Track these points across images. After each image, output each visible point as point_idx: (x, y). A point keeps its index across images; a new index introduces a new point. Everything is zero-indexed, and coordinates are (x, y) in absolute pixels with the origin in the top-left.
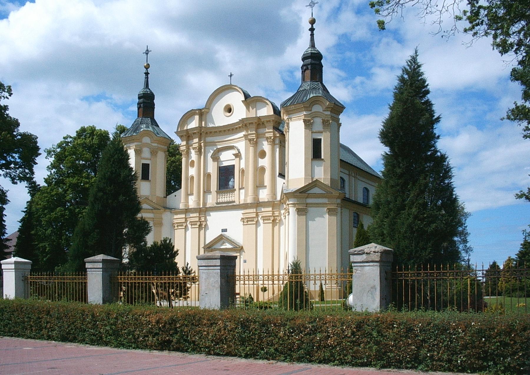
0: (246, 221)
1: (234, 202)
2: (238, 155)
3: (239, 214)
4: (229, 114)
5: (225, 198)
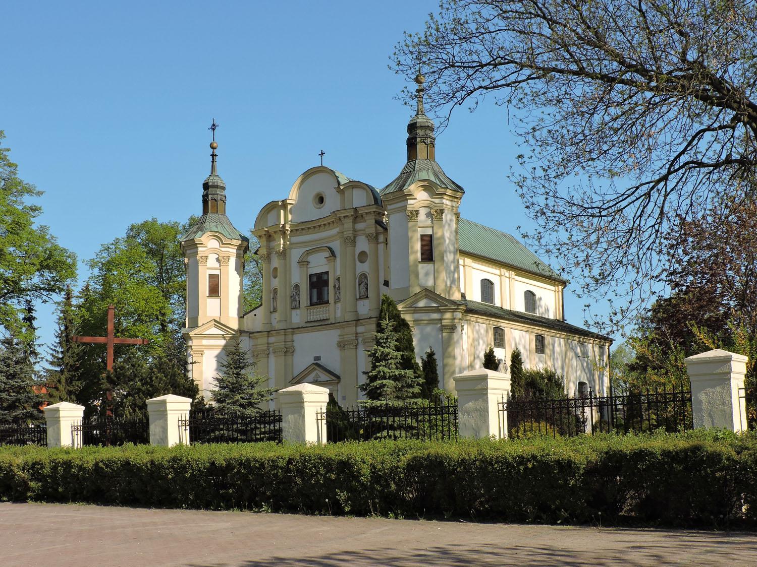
4: (322, 205)
5: (319, 313)
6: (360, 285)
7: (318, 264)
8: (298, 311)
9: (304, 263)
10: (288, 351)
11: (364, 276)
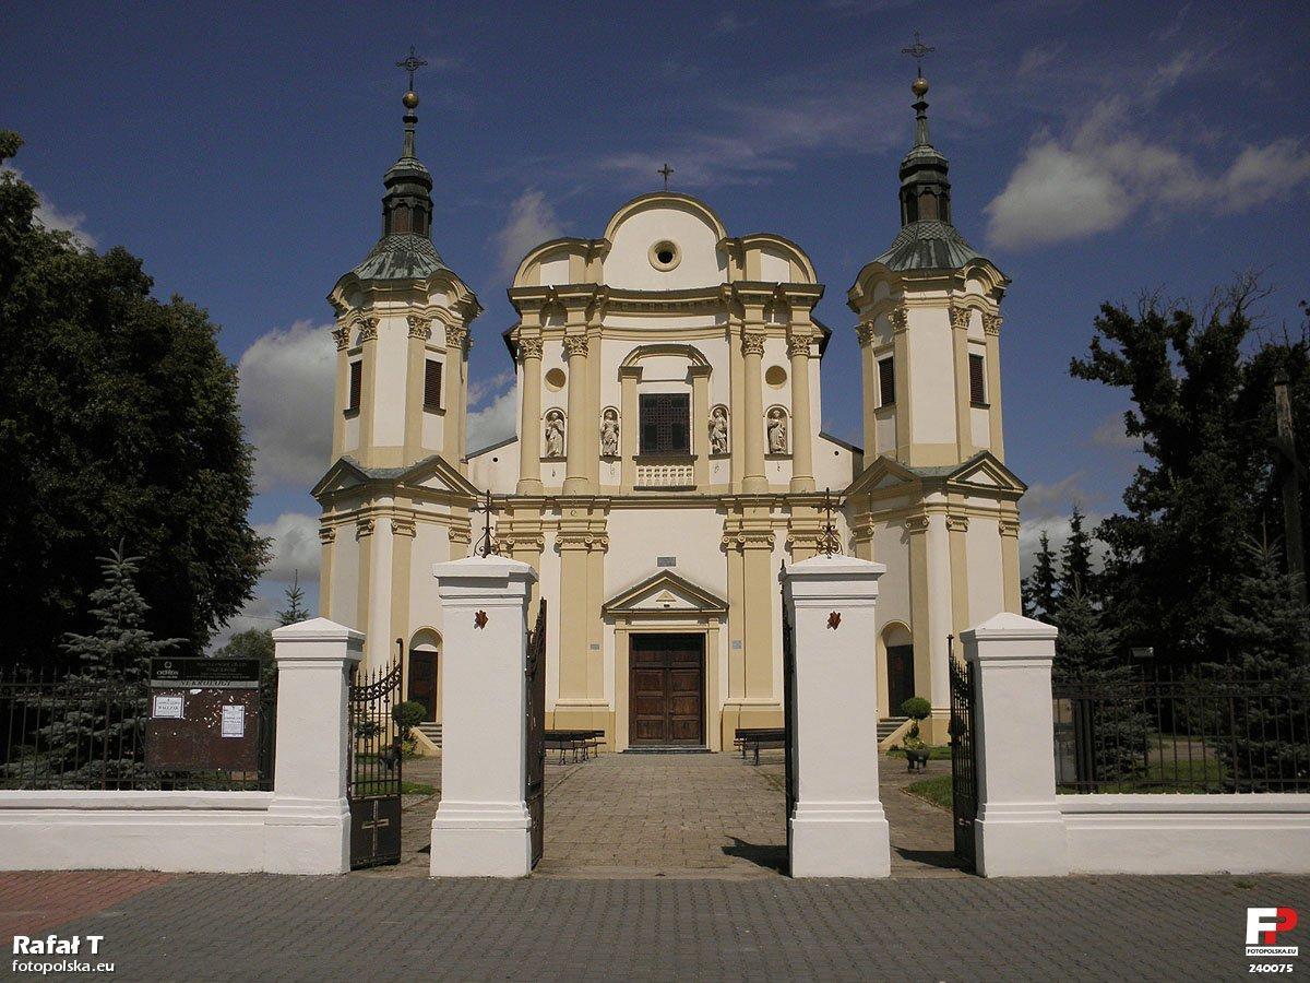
0: (735, 543)
1: (694, 488)
2: (701, 370)
3: (711, 522)
4: (663, 266)
6: (769, 429)
7: (666, 374)
8: (617, 464)
9: (629, 372)
10: (596, 543)
11: (776, 413)
